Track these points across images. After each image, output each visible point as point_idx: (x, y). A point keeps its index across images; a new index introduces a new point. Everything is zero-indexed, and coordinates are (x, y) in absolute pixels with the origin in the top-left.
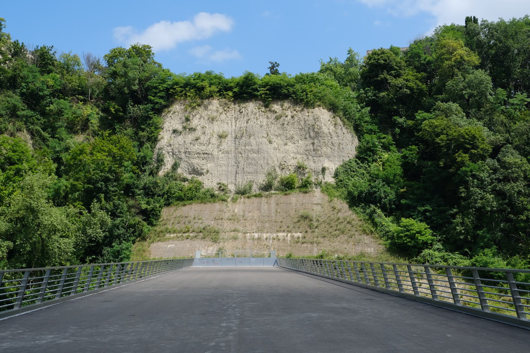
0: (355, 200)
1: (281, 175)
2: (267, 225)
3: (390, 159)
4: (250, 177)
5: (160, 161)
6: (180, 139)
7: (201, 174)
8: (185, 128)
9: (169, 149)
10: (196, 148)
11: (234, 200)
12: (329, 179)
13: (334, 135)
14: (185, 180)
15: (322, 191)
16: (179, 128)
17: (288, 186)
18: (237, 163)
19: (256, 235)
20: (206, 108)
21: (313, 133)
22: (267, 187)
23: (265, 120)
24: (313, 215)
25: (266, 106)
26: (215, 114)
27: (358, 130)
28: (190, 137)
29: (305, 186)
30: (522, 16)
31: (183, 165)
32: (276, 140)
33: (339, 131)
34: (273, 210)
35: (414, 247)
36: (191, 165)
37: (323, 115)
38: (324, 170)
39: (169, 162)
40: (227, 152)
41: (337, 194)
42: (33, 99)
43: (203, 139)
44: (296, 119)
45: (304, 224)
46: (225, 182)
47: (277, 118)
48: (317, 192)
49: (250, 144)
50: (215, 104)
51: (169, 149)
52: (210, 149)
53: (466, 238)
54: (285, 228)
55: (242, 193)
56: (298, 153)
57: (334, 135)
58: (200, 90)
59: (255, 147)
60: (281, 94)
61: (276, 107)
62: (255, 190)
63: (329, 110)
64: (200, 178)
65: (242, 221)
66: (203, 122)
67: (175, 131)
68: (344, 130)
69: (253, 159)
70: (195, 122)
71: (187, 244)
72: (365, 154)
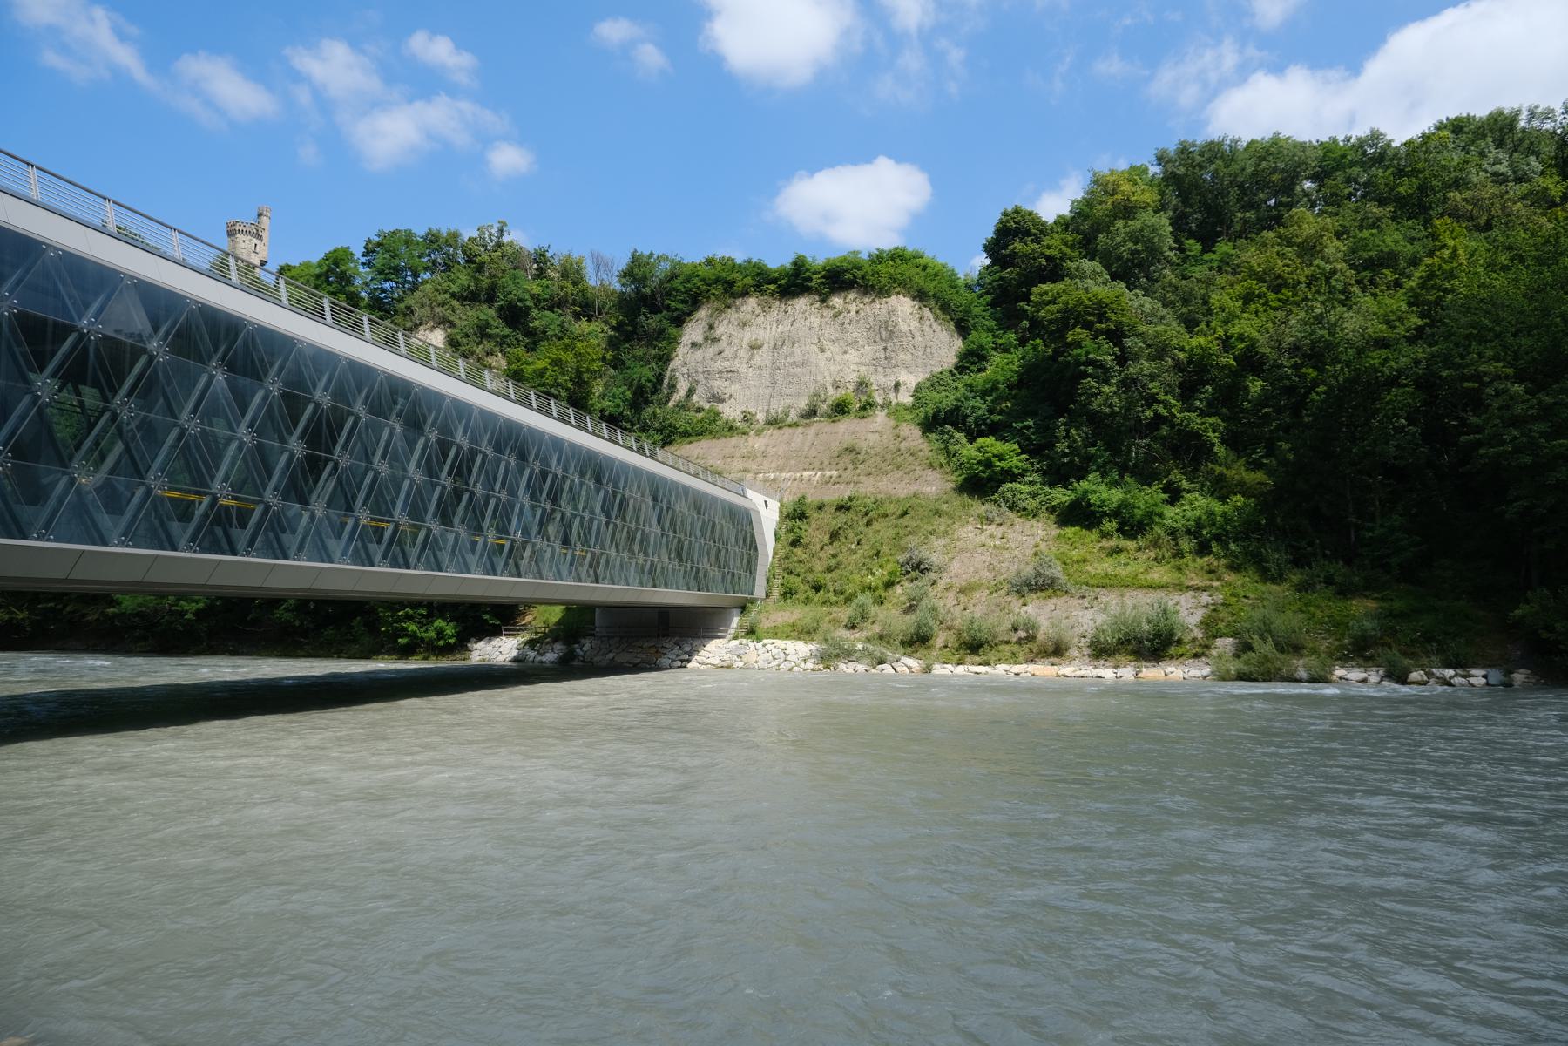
0: (932, 424)
1: (833, 395)
2: (792, 462)
3: (1002, 366)
4: (788, 401)
5: (673, 387)
6: (699, 354)
7: (723, 401)
8: (706, 339)
9: (684, 370)
10: (719, 365)
11: (759, 433)
12: (906, 398)
13: (917, 334)
14: (699, 410)
15: (888, 415)
16: (699, 339)
17: (840, 409)
18: (773, 382)
19: (772, 476)
20: (738, 309)
21: (886, 333)
22: (812, 413)
23: (818, 321)
24: (863, 446)
25: (823, 301)
26: (748, 317)
27: (963, 328)
28: (712, 350)
29: (867, 407)
30: (1268, 136)
31: (700, 390)
32: (826, 347)
33: (926, 328)
34: (808, 443)
35: (990, 479)
36: (710, 389)
37: (902, 307)
38: (897, 386)
39: (683, 387)
40: (760, 368)
41: (908, 417)
42: (515, 316)
43: (728, 352)
44: (862, 314)
45: (846, 460)
46: (752, 410)
47: (835, 316)
48: (880, 418)
49: (792, 355)
50: (752, 302)
51: (684, 370)
52: (735, 365)
53: (1072, 461)
54: (817, 465)
55: (773, 422)
56: (862, 364)
57: (917, 334)
58: (729, 285)
59: (798, 359)
60: (844, 282)
61: (836, 301)
62: (793, 417)
63: (914, 298)
64: (720, 407)
65: (760, 458)
66: (731, 329)
67: (694, 345)
68: (936, 327)
69: (795, 375)
70: (720, 330)
71: (1478, 837)
72: (971, 359)
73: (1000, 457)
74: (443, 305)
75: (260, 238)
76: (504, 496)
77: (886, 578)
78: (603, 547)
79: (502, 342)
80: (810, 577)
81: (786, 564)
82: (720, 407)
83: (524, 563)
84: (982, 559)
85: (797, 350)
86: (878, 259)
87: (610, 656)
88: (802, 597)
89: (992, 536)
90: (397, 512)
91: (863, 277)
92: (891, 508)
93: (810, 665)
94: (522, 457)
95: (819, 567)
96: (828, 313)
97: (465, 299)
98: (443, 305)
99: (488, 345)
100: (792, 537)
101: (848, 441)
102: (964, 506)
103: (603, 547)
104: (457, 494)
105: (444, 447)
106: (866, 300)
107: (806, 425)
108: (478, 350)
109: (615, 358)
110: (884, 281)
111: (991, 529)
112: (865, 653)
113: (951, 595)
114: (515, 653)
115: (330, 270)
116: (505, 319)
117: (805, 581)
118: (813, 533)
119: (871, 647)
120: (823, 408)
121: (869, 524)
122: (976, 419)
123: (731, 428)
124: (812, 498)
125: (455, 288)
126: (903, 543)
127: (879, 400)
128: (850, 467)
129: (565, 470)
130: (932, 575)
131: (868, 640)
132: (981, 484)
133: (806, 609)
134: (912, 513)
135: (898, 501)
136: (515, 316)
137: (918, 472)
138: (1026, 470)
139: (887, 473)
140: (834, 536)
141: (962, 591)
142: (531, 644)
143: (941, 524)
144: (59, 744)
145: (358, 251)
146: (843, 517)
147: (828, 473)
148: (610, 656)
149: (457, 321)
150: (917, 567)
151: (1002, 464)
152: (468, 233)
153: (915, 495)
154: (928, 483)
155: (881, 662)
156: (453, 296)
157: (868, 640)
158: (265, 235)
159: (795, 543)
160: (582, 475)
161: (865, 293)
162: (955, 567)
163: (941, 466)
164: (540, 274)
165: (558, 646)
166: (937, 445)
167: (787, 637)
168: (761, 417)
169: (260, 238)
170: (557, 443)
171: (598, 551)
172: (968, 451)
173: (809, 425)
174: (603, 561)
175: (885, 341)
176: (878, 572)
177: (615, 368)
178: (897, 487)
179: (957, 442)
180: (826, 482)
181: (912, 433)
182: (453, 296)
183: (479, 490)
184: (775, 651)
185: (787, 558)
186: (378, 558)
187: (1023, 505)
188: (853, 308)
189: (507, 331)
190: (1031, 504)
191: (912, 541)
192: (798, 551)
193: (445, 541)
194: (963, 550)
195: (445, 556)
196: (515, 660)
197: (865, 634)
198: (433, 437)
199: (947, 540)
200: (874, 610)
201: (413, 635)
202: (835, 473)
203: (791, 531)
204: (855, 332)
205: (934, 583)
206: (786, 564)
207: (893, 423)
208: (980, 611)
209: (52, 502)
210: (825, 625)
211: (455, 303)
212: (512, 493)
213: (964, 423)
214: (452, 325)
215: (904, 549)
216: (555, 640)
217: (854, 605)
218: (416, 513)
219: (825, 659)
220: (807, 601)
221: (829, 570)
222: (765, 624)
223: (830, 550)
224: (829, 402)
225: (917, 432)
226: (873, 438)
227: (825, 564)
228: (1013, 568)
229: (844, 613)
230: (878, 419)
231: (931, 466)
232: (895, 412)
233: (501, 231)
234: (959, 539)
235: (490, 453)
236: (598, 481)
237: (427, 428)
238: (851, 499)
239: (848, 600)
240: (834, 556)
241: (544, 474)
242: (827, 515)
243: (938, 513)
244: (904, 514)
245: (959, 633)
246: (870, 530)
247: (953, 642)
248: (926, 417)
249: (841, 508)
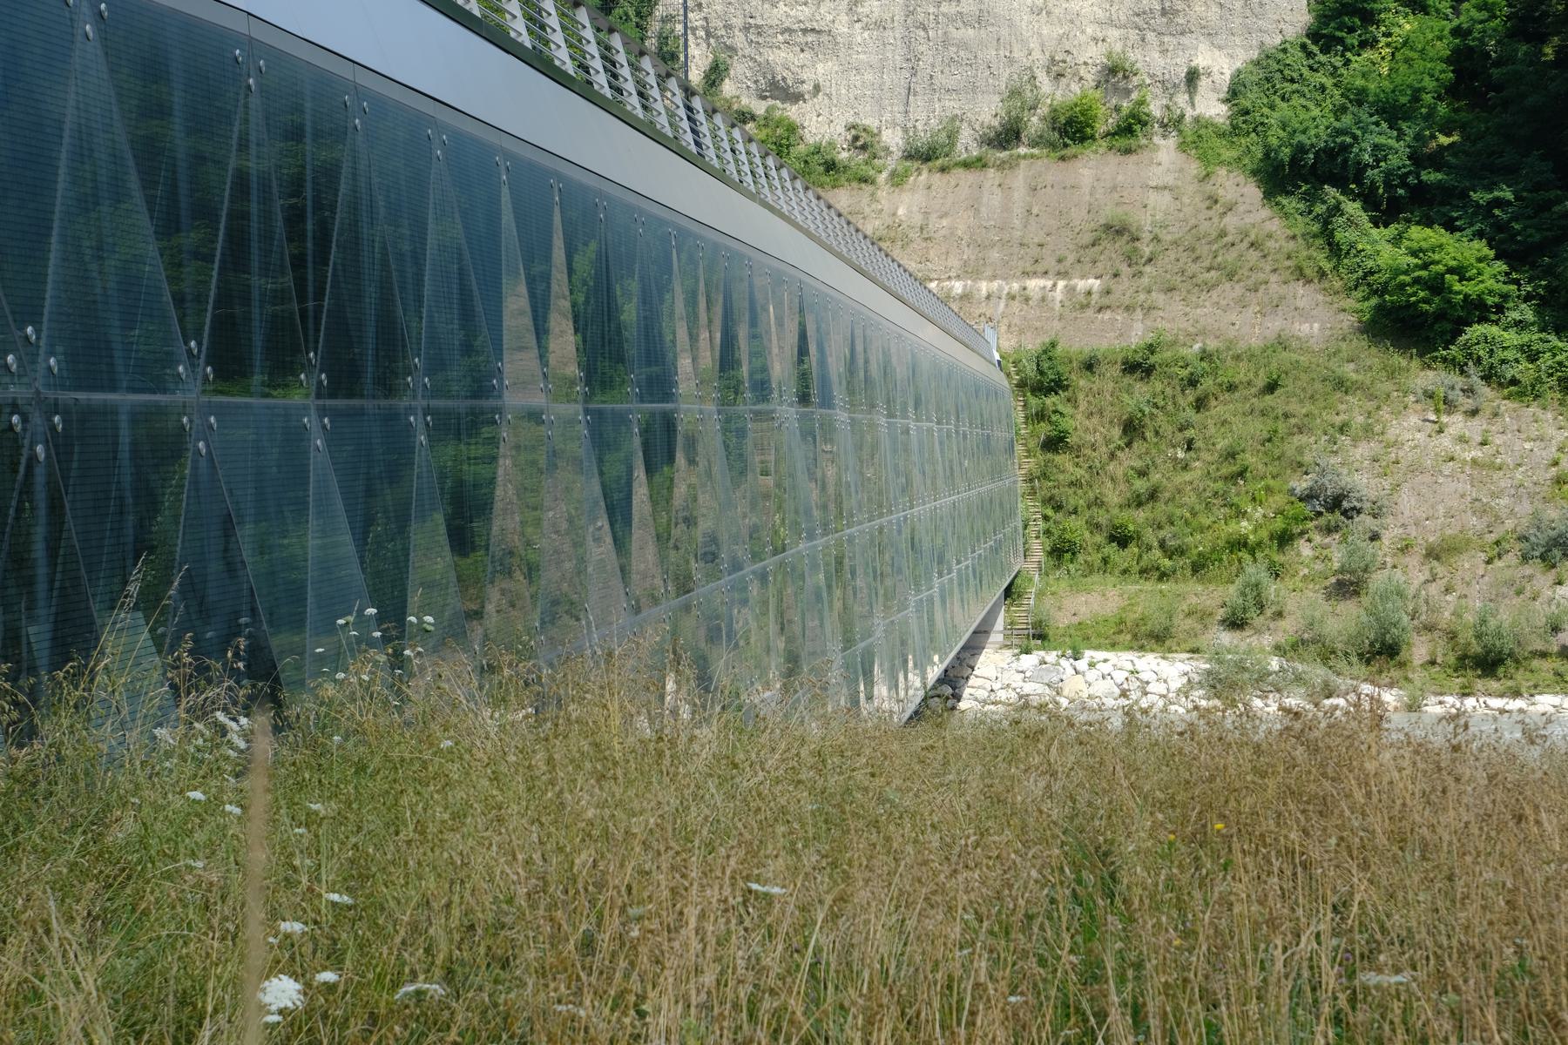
0: (1285, 175)
1: (1054, 94)
2: (995, 255)
4: (952, 105)
7: (797, 98)
11: (897, 179)
12: (1211, 107)
15: (1183, 147)
17: (1072, 130)
18: (912, 60)
19: (958, 287)
22: (1007, 136)
24: (1144, 221)
29: (1130, 128)
31: (739, 68)
34: (1018, 209)
35: (1440, 316)
36: (765, 68)
38: (1192, 77)
40: (880, 25)
41: (1229, 154)
45: (1113, 250)
46: (871, 122)
48: (1165, 150)
54: (1049, 262)
55: (924, 155)
56: (1111, 23)
64: (792, 112)
65: (918, 244)
69: (962, 45)
73: (1460, 272)
81: (1045, 488)
82: (792, 112)
84: (1454, 489)
89: (1462, 440)
92: (1241, 373)
95: (1113, 497)
100: (1044, 429)
102: (1392, 374)
111: (1456, 423)
113: (1413, 561)
117: (1095, 527)
120: (1034, 124)
121: (1200, 404)
122: (1388, 174)
123: (830, 166)
124: (1077, 341)
126: (1289, 449)
127: (1155, 109)
130: (1365, 521)
132: (1415, 322)
134: (1288, 384)
138: (1505, 297)
140: (1132, 429)
141: (1433, 554)
143: (1353, 409)
147: (1081, 285)
150: (1335, 503)
151: (1470, 288)
153: (1282, 343)
154: (1304, 315)
159: (1054, 443)
162: (1407, 502)
166: (1301, 225)
167: (1113, 646)
168: (893, 139)
172: (1385, 248)
179: (1351, 222)
180: (1083, 304)
185: (1045, 476)
187: (1509, 373)
190: (1523, 370)
192: (1062, 459)
194: (1415, 469)
203: (1041, 416)
205: (1375, 537)
206: (1045, 488)
208: (1474, 596)
213: (1358, 180)
221: (1138, 502)
222: (1061, 621)
223: (1129, 460)
224: (1043, 110)
225: (1252, 192)
226: (1160, 202)
228: (1525, 508)
231: (1299, 273)
232: (1196, 138)
240: (1142, 474)
243: (1341, 385)
244: (1271, 387)
249: (1137, 367)
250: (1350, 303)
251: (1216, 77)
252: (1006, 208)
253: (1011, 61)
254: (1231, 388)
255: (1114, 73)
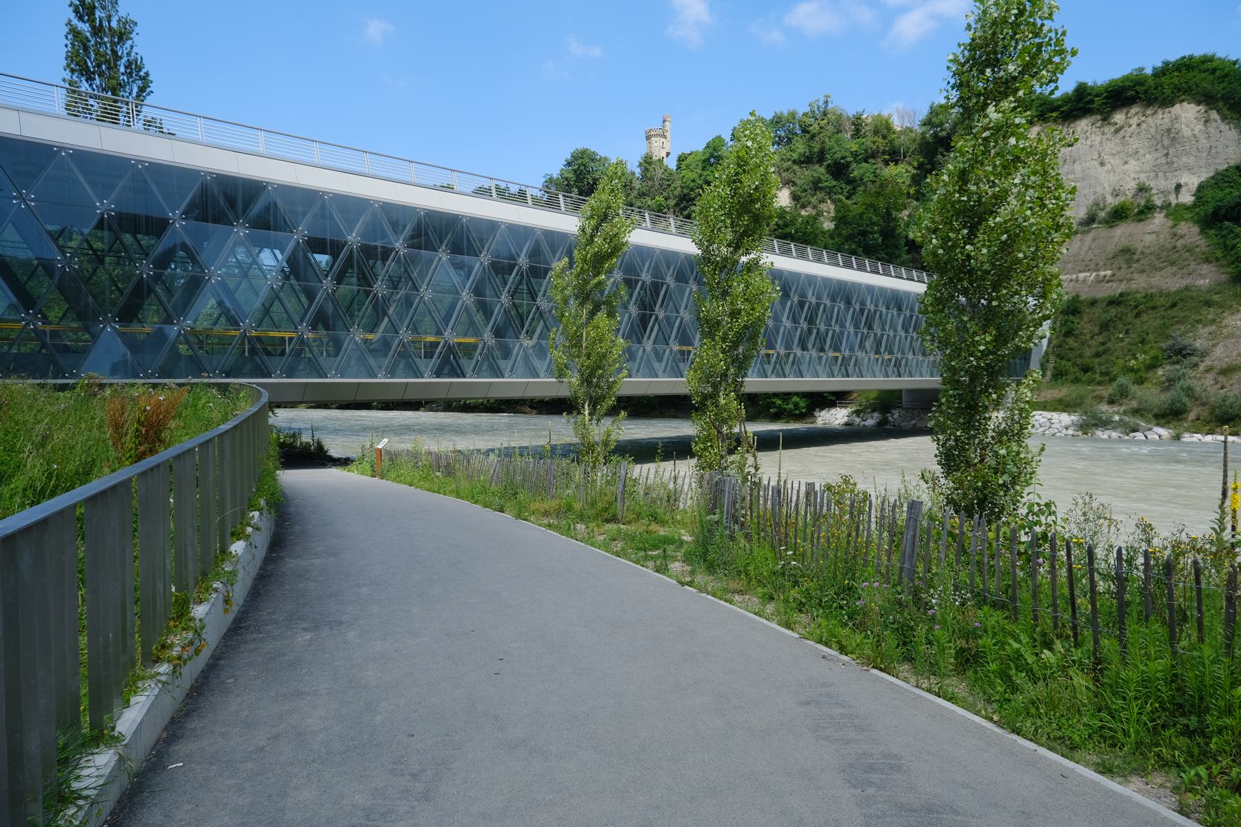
1: (1112, 202)
2: (1070, 266)
12: (1187, 198)
15: (1167, 216)
21: (1171, 136)
22: (1091, 220)
24: (1139, 247)
29: (1147, 210)
33: (1212, 130)
34: (1085, 248)
38: (1178, 187)
41: (1187, 216)
44: (1144, 126)
45: (1121, 261)
47: (1117, 131)
48: (1159, 219)
49: (1073, 172)
54: (1092, 266)
56: (1142, 171)
61: (1119, 117)
68: (1224, 127)
74: (787, 170)
75: (665, 137)
76: (837, 329)
77: (1148, 362)
78: (903, 353)
79: (830, 192)
80: (1079, 361)
83: (850, 369)
85: (1077, 167)
86: (1164, 71)
87: (913, 422)
88: (1071, 377)
90: (778, 346)
91: (1146, 92)
93: (1070, 432)
94: (848, 302)
95: (1088, 352)
96: (1109, 130)
97: (803, 162)
98: (787, 170)
99: (820, 195)
101: (1124, 243)
103: (903, 353)
104: (810, 332)
105: (801, 304)
106: (1149, 112)
107: (1084, 233)
108: (813, 200)
109: (918, 192)
110: (1167, 91)
112: (1121, 424)
113: (1210, 376)
114: (846, 419)
115: (712, 155)
116: (832, 174)
117: (1074, 364)
118: (1085, 326)
119: (1126, 419)
121: (1138, 315)
125: (795, 156)
127: (1159, 203)
128: (1124, 266)
129: (876, 306)
130: (1195, 359)
131: (1125, 413)
133: (1073, 388)
134: (1181, 304)
135: (1168, 295)
136: (839, 170)
137: (1192, 267)
139: (1161, 269)
140: (1105, 326)
142: (857, 413)
143: (1211, 313)
144: (813, 450)
145: (727, 137)
146: (1113, 311)
147: (1102, 273)
148: (913, 422)
149: (798, 181)
152: (802, 109)
153: (1187, 288)
154: (1203, 277)
155: (1134, 431)
156: (794, 162)
157: (1125, 413)
158: (667, 134)
159: (1069, 333)
160: (888, 308)
161: (1148, 106)
162: (1219, 351)
163: (1217, 259)
164: (857, 133)
165: (876, 415)
166: (1216, 240)
167: (1055, 410)
169: (665, 137)
170: (870, 289)
171: (899, 356)
173: (1089, 231)
174: (903, 363)
175: (1167, 148)
176: (1141, 357)
177: (917, 200)
178: (1169, 281)
181: (1190, 232)
182: (794, 162)
183: (823, 328)
184: (1042, 420)
185: (1060, 346)
186: (769, 373)
188: (1134, 121)
189: (834, 183)
191: (1176, 331)
192: (1071, 341)
193: (804, 358)
195: (804, 368)
196: (846, 424)
197: (1123, 409)
198: (796, 300)
199: (1213, 328)
200: (1134, 388)
201: (779, 407)
202: (1109, 273)
204: (1135, 144)
205: (1196, 365)
207: (1170, 223)
209: (638, 360)
210: (1088, 401)
211: (796, 167)
212: (842, 326)
214: (794, 184)
215: (1168, 337)
216: (874, 411)
217: (1115, 385)
218: (788, 347)
219: (1084, 428)
220: (1076, 381)
221: (1098, 355)
223: (1100, 339)
224: (1108, 209)
225: (1196, 229)
226: (1148, 239)
227: (1093, 351)
229: (1107, 391)
230: (1157, 221)
231: (1207, 261)
232: (1175, 213)
233: (826, 102)
234: (1226, 326)
235: (828, 303)
236: (900, 309)
237: (792, 294)
238: (1121, 295)
239: (1113, 380)
240: (1103, 344)
241: (862, 311)
242: (1097, 310)
244: (1174, 305)
245: (1213, 408)
246: (1138, 322)
247: (1205, 413)
248: (1206, 215)
249: (1112, 302)
250: (1229, 270)
251: (1190, 186)
252: (1080, 248)
253: (1095, 193)
254: (1154, 308)
255: (1142, 189)
